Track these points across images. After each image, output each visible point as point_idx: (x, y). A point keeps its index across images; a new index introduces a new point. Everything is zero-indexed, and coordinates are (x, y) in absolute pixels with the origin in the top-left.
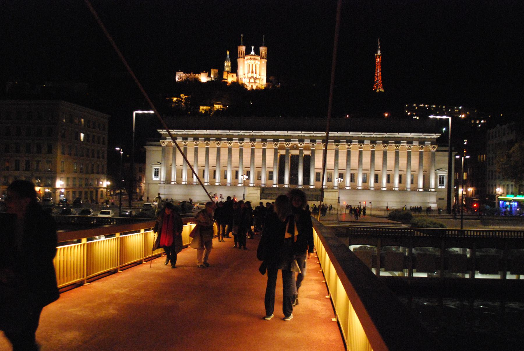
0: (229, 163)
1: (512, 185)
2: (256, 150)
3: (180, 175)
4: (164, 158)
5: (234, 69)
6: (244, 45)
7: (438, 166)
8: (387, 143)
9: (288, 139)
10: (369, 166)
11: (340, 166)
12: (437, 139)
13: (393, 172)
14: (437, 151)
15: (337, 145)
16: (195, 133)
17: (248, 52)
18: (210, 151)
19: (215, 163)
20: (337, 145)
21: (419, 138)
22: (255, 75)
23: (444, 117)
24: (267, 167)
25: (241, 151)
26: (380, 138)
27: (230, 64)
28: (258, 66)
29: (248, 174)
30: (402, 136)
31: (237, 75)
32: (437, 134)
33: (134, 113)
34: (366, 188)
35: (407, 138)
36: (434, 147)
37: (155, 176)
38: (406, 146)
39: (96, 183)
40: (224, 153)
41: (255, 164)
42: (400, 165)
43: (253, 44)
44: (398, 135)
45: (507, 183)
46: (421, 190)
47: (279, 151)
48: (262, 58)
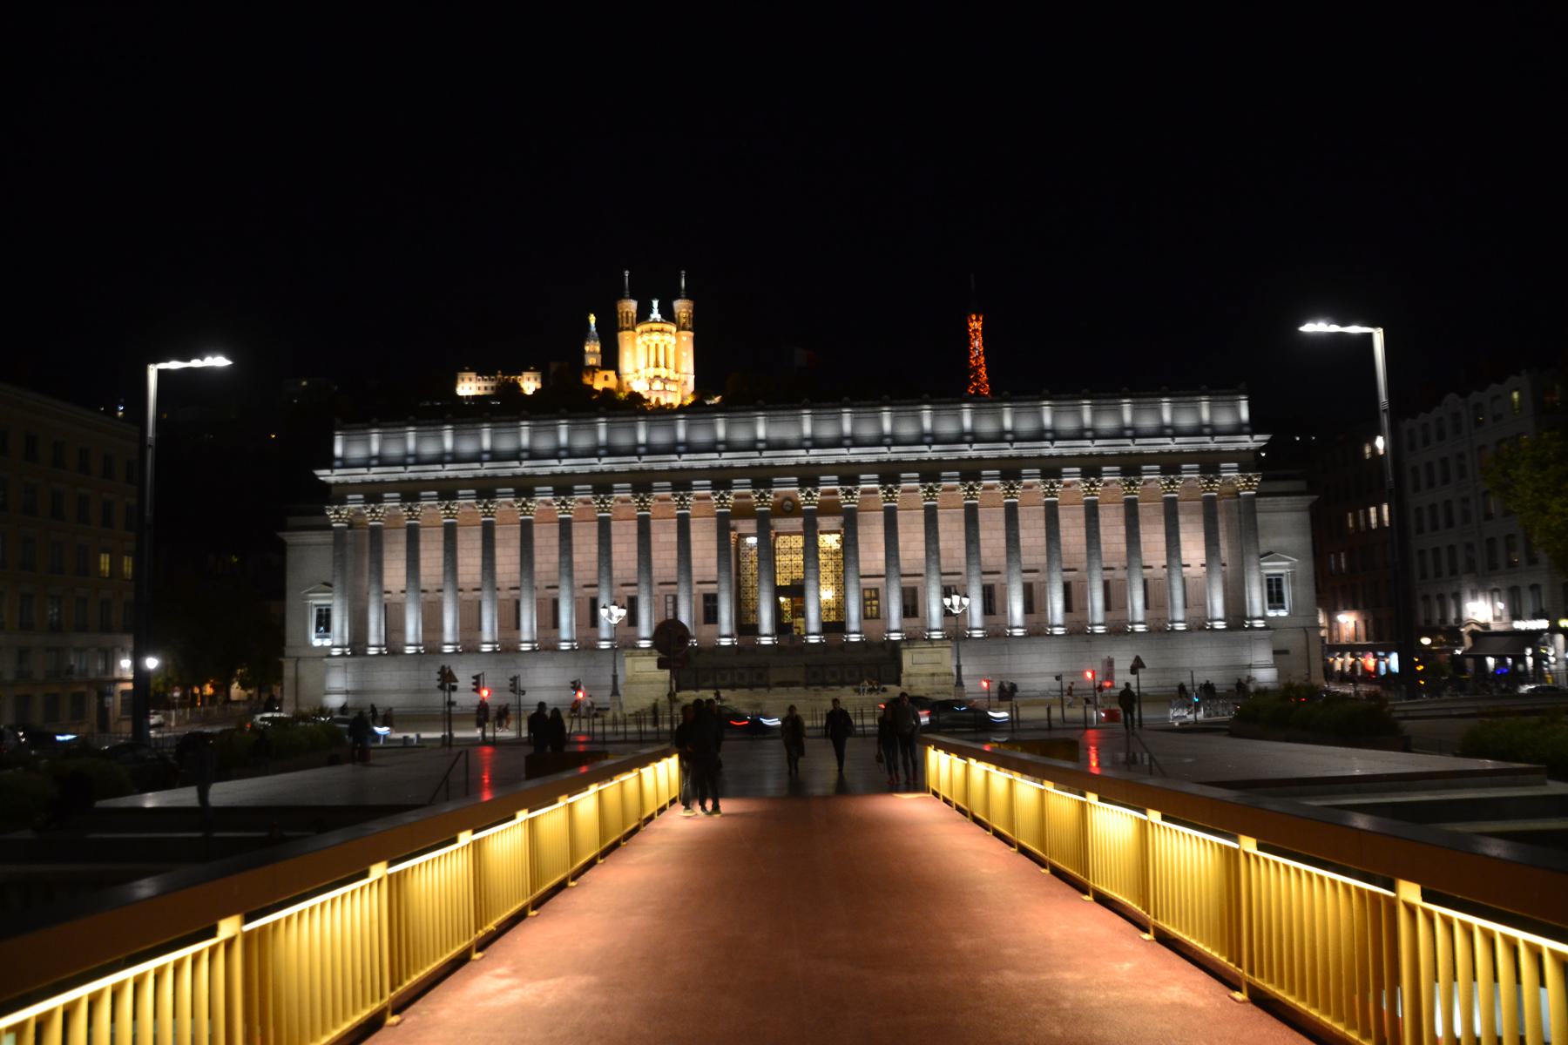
0: (565, 570)
1: (1535, 588)
3: (394, 627)
4: (343, 568)
5: (611, 359)
6: (632, 297)
8: (1098, 474)
10: (1043, 559)
11: (1027, 560)
15: (931, 489)
16: (442, 474)
17: (643, 315)
18: (498, 535)
19: (517, 576)
22: (663, 372)
23: (1355, 329)
24: (695, 579)
25: (604, 527)
27: (598, 349)
28: (671, 349)
29: (632, 606)
30: (1146, 449)
31: (618, 375)
32: (1257, 437)
33: (153, 371)
34: (1037, 630)
36: (1250, 479)
39: (100, 666)
41: (655, 572)
43: (655, 291)
45: (1533, 581)
47: (733, 523)
48: (681, 328)
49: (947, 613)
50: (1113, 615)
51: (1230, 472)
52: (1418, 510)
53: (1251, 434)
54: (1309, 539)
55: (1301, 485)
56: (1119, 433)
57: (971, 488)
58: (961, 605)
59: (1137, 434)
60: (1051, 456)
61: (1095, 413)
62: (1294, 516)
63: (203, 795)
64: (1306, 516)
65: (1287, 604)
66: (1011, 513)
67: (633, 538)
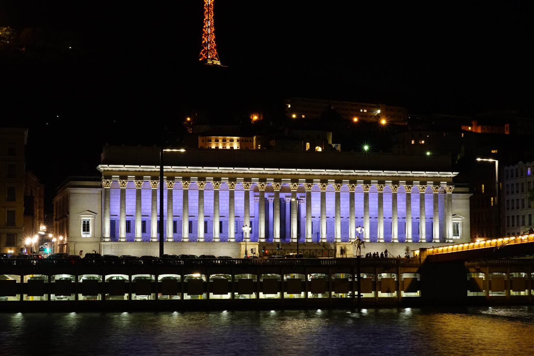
2: (236, 193)
7: (456, 211)
9: (278, 179)
11: (252, 212)
12: (454, 178)
13: (226, 219)
14: (453, 193)
20: (339, 186)
21: (434, 177)
26: (331, 177)
32: (454, 173)
35: (420, 177)
36: (450, 188)
37: (84, 230)
40: (193, 196)
42: (327, 209)
44: (410, 174)
46: (382, 241)
49: (356, 233)
51: (444, 185)
54: (469, 210)
55: (467, 189)
58: (361, 230)
60: (382, 176)
66: (366, 196)
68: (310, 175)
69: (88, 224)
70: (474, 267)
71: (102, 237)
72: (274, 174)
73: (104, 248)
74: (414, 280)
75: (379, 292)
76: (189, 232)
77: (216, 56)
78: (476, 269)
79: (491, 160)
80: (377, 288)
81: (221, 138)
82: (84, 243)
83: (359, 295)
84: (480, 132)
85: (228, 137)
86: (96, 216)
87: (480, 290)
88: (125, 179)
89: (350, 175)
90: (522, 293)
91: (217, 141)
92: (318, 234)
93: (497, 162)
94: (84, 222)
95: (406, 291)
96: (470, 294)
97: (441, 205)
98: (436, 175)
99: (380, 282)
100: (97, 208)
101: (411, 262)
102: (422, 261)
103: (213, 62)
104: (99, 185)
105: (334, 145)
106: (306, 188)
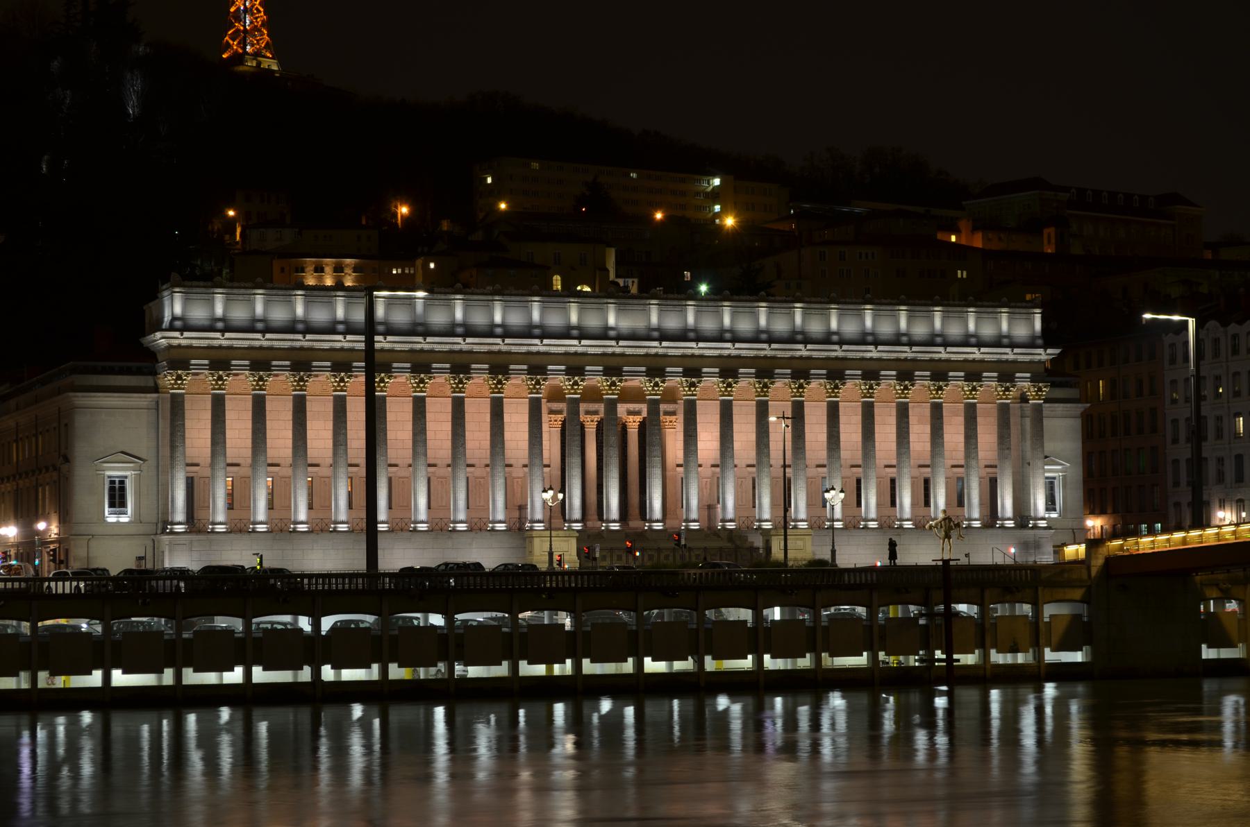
11: (845, 454)
14: (1047, 401)
20: (765, 386)
32: (1049, 351)
35: (966, 361)
36: (1040, 389)
37: (112, 505)
38: (208, 377)
42: (469, 445)
50: (236, 514)
51: (1024, 383)
52: (1175, 421)
53: (1045, 347)
54: (1079, 445)
56: (930, 342)
57: (220, 378)
59: (309, 329)
60: (871, 359)
61: (910, 319)
62: (1069, 422)
63: (550, 669)
64: (1077, 424)
65: (1058, 507)
67: (857, 419)
68: (693, 356)
69: (123, 489)
70: (1217, 585)
71: (164, 524)
72: (604, 354)
73: (170, 551)
74: (1076, 618)
75: (648, 661)
76: (390, 508)
77: (267, 46)
78: (1221, 590)
79: (1176, 318)
80: (988, 640)
81: (329, 262)
82: (114, 535)
83: (949, 660)
84: (980, 246)
85: (348, 261)
86: (145, 467)
87: (1230, 644)
88: (305, 371)
89: (792, 358)
90: (557, 669)
91: (319, 269)
92: (522, 508)
93: (1191, 322)
94: (113, 482)
95: (1057, 648)
96: (1208, 653)
97: (1019, 436)
98: (1005, 357)
99: (826, 629)
100: (144, 446)
101: (1066, 575)
102: (1094, 571)
103: (259, 63)
104: (151, 384)
105: (621, 282)
106: (684, 393)
